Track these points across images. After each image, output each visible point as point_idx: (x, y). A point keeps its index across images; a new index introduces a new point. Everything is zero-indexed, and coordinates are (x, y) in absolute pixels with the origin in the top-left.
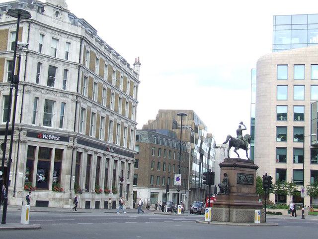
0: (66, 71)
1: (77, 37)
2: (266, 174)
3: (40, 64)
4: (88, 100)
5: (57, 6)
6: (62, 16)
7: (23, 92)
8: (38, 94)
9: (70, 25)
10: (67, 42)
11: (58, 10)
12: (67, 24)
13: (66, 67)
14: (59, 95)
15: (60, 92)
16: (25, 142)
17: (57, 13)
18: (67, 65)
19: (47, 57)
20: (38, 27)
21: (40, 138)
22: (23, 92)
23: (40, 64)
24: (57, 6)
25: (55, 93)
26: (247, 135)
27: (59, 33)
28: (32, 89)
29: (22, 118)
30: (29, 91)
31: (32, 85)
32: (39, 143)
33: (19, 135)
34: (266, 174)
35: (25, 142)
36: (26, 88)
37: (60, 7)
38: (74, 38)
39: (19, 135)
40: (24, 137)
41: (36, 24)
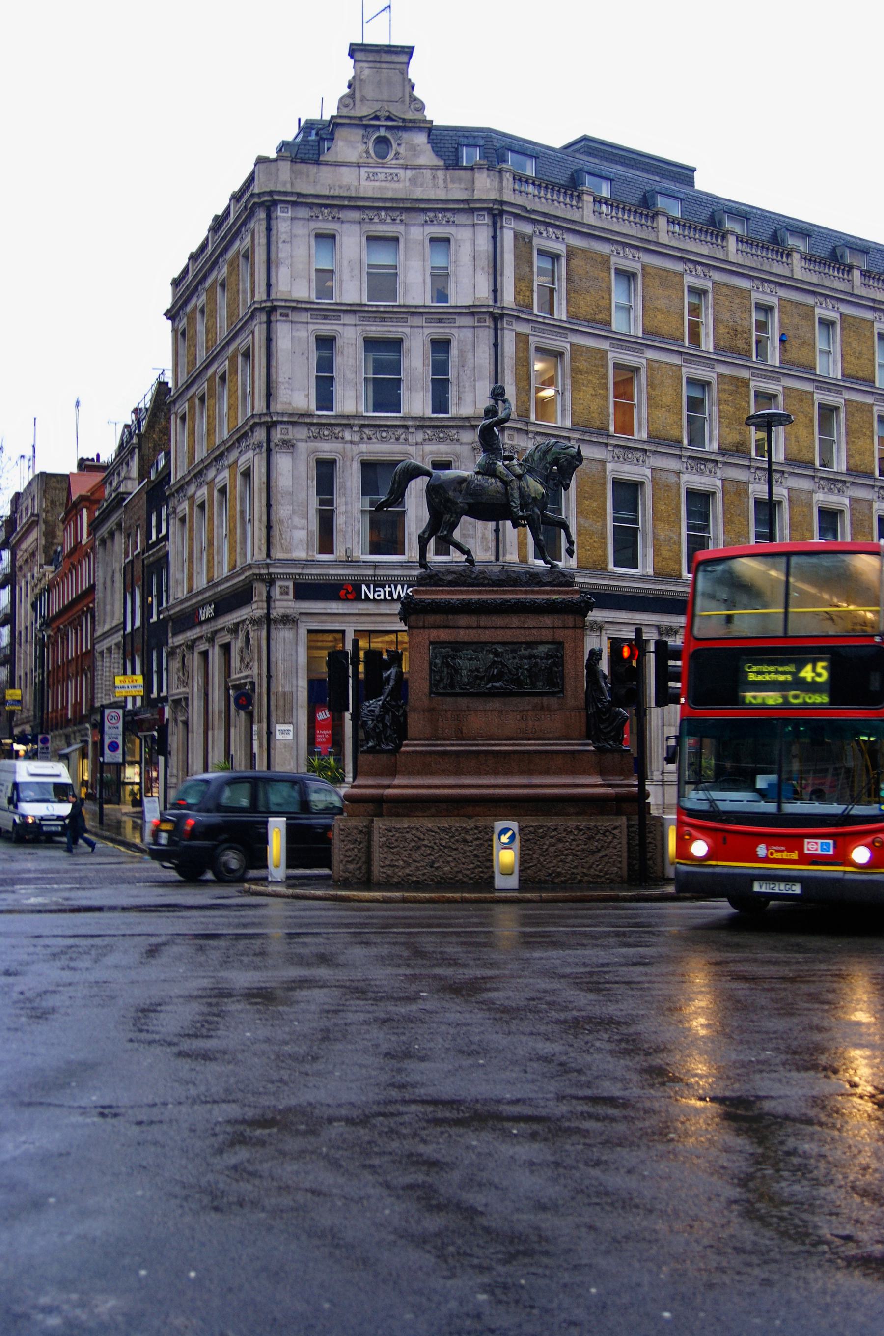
0: (440, 346)
1: (472, 211)
2: (98, 456)
3: (326, 343)
4: (652, 448)
5: (377, 118)
6: (402, 150)
7: (269, 450)
8: (327, 448)
9: (440, 174)
10: (369, 238)
11: (382, 132)
12: (428, 173)
13: (438, 331)
14: (420, 436)
15: (419, 427)
16: (287, 620)
17: (382, 142)
18: (440, 321)
19: (353, 310)
20: (303, 213)
21: (346, 600)
22: (269, 450)
23: (326, 343)
24: (377, 118)
25: (400, 431)
26: (583, 184)
27: (394, 214)
28: (301, 433)
29: (273, 541)
30: (288, 445)
31: (299, 419)
32: (353, 618)
33: (269, 598)
34: (98, 456)
35: (287, 620)
36: (278, 435)
37: (388, 118)
38: (461, 219)
39: (269, 598)
40: (285, 604)
41: (294, 204)
